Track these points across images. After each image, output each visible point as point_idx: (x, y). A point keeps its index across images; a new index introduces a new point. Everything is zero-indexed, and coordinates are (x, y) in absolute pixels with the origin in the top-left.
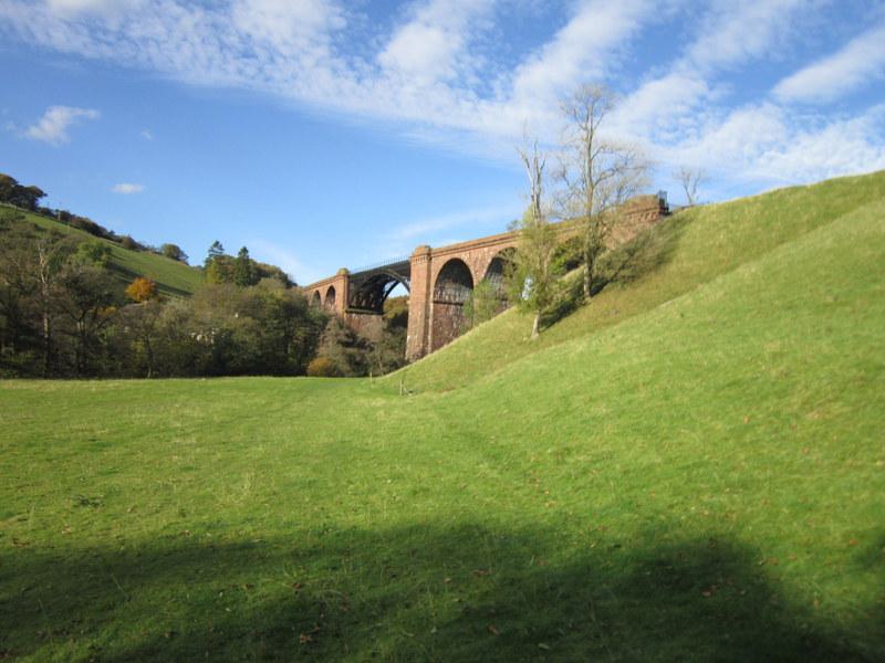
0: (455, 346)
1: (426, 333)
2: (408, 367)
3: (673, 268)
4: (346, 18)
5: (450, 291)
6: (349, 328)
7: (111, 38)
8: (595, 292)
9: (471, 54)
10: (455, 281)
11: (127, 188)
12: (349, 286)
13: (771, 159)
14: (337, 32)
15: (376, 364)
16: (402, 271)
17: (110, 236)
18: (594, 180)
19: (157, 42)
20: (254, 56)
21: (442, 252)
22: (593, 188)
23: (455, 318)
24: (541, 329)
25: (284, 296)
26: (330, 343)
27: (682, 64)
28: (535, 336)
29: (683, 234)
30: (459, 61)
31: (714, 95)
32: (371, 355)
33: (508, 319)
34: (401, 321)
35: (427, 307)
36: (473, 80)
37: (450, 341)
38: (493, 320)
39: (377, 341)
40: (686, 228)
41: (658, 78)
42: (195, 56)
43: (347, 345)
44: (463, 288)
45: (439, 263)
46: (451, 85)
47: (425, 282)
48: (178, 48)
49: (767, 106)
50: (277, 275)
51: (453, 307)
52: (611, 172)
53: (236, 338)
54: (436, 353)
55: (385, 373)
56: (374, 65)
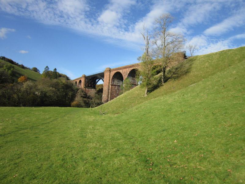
0: (119, 98)
2: (103, 105)
3: (191, 74)
5: (116, 82)
6: (85, 92)
7: (23, 10)
8: (165, 81)
9: (123, 19)
11: (23, 52)
12: (85, 80)
13: (203, 50)
14: (87, 11)
16: (101, 76)
17: (17, 64)
18: (166, 45)
19: (36, 12)
20: (63, 17)
21: (114, 70)
22: (165, 47)
23: (117, 90)
24: (148, 93)
25: (66, 82)
26: (79, 97)
27: (180, 24)
28: (146, 95)
29: (193, 64)
30: (120, 21)
31: (189, 33)
32: (91, 101)
33: (136, 90)
34: (101, 91)
35: (109, 86)
36: (124, 26)
37: (116, 97)
38: (130, 90)
39: (93, 96)
40: (193, 62)
41: (173, 27)
42: (47, 17)
43: (84, 97)
44: (120, 81)
45: (113, 73)
46: (118, 27)
47: (108, 79)
49: (202, 36)
50: (65, 77)
51: (117, 87)
52: (171, 43)
53: (48, 94)
54: (112, 101)
55: (96, 107)
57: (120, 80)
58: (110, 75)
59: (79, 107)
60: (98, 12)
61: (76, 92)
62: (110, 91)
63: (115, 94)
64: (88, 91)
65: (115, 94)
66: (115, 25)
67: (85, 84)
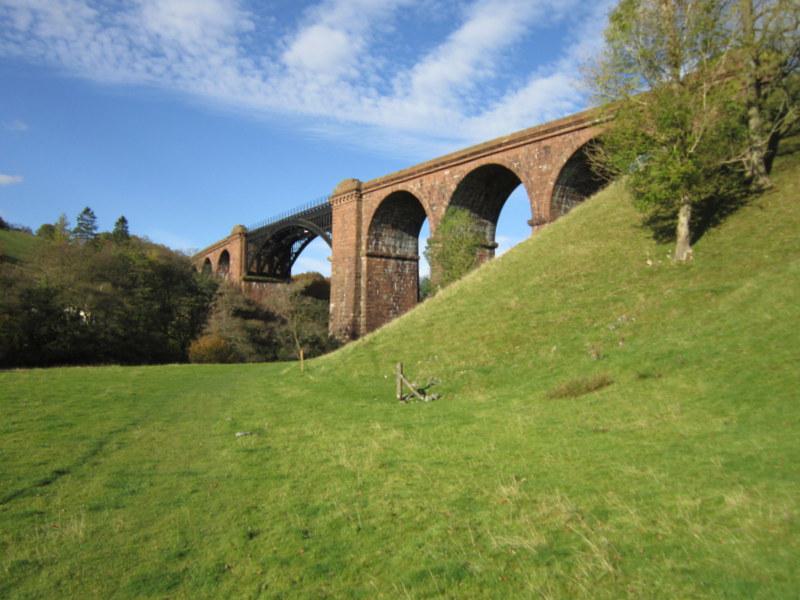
1: (357, 299)
4: (255, 21)
5: (389, 241)
7: (20, 37)
9: (373, 55)
10: (395, 227)
12: (247, 247)
15: (291, 342)
16: (317, 222)
19: (66, 41)
20: (163, 55)
21: (377, 186)
23: (396, 278)
26: (223, 313)
27: (566, 64)
30: (361, 61)
32: (283, 329)
35: (358, 262)
36: (374, 79)
41: (545, 76)
44: (406, 236)
45: (373, 201)
46: (353, 83)
47: (354, 227)
48: (88, 47)
51: (392, 262)
56: (280, 64)
57: (405, 230)
58: (359, 212)
59: (230, 362)
60: (285, 33)
61: (211, 296)
62: (363, 283)
63: (385, 297)
64: (261, 292)
65: (385, 297)
66: (344, 78)
67: (246, 263)
